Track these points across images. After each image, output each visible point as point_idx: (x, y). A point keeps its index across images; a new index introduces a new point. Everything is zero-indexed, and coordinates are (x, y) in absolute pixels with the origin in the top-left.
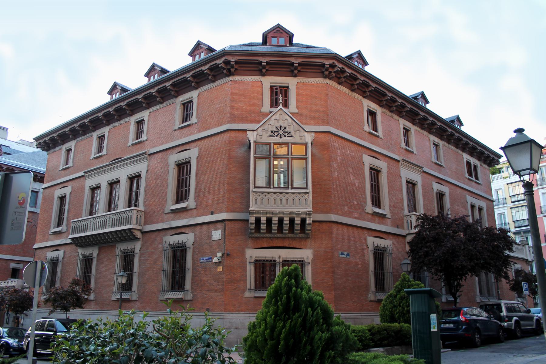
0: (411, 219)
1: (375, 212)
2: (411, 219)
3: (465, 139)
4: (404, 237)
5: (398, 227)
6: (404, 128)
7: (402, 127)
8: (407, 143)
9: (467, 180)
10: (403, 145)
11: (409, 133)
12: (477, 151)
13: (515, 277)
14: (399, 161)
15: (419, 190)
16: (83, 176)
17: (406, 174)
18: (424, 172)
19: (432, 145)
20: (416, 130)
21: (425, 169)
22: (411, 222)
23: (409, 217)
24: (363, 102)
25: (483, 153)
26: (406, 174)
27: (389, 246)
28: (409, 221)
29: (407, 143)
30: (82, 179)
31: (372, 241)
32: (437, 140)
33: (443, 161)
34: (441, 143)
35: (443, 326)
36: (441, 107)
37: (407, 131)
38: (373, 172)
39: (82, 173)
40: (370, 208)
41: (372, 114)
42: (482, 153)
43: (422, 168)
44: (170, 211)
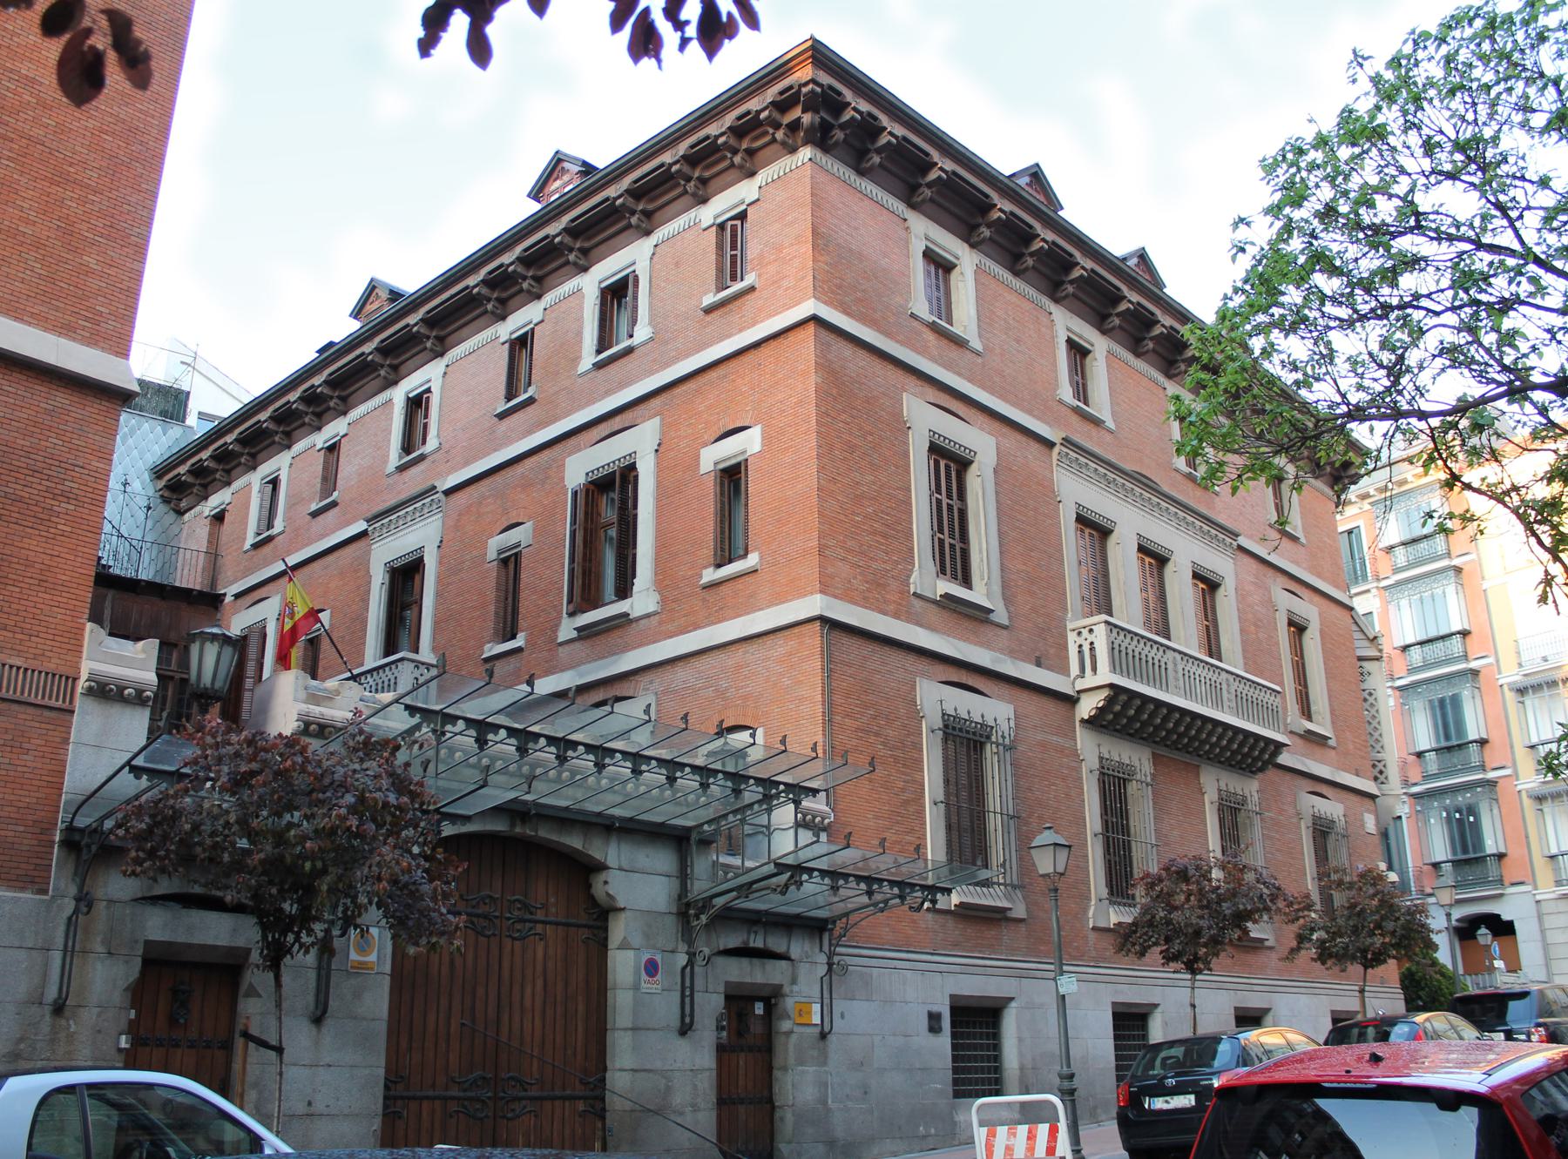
0: (1091, 638)
1: (1309, 732)
2: (1091, 638)
5: (1039, 664)
6: (1070, 342)
7: (918, 247)
8: (1081, 391)
10: (1066, 393)
11: (1089, 359)
14: (1050, 445)
15: (1226, 602)
16: (364, 534)
18: (1240, 548)
19: (918, 264)
20: (979, 270)
21: (1242, 541)
22: (1092, 649)
23: (1085, 632)
24: (1054, 316)
26: (1076, 490)
27: (1004, 727)
28: (1086, 648)
29: (1081, 391)
30: (361, 544)
34: (1100, 345)
35: (759, 1009)
37: (940, 266)
38: (1147, 560)
39: (361, 526)
41: (1078, 352)
44: (574, 634)
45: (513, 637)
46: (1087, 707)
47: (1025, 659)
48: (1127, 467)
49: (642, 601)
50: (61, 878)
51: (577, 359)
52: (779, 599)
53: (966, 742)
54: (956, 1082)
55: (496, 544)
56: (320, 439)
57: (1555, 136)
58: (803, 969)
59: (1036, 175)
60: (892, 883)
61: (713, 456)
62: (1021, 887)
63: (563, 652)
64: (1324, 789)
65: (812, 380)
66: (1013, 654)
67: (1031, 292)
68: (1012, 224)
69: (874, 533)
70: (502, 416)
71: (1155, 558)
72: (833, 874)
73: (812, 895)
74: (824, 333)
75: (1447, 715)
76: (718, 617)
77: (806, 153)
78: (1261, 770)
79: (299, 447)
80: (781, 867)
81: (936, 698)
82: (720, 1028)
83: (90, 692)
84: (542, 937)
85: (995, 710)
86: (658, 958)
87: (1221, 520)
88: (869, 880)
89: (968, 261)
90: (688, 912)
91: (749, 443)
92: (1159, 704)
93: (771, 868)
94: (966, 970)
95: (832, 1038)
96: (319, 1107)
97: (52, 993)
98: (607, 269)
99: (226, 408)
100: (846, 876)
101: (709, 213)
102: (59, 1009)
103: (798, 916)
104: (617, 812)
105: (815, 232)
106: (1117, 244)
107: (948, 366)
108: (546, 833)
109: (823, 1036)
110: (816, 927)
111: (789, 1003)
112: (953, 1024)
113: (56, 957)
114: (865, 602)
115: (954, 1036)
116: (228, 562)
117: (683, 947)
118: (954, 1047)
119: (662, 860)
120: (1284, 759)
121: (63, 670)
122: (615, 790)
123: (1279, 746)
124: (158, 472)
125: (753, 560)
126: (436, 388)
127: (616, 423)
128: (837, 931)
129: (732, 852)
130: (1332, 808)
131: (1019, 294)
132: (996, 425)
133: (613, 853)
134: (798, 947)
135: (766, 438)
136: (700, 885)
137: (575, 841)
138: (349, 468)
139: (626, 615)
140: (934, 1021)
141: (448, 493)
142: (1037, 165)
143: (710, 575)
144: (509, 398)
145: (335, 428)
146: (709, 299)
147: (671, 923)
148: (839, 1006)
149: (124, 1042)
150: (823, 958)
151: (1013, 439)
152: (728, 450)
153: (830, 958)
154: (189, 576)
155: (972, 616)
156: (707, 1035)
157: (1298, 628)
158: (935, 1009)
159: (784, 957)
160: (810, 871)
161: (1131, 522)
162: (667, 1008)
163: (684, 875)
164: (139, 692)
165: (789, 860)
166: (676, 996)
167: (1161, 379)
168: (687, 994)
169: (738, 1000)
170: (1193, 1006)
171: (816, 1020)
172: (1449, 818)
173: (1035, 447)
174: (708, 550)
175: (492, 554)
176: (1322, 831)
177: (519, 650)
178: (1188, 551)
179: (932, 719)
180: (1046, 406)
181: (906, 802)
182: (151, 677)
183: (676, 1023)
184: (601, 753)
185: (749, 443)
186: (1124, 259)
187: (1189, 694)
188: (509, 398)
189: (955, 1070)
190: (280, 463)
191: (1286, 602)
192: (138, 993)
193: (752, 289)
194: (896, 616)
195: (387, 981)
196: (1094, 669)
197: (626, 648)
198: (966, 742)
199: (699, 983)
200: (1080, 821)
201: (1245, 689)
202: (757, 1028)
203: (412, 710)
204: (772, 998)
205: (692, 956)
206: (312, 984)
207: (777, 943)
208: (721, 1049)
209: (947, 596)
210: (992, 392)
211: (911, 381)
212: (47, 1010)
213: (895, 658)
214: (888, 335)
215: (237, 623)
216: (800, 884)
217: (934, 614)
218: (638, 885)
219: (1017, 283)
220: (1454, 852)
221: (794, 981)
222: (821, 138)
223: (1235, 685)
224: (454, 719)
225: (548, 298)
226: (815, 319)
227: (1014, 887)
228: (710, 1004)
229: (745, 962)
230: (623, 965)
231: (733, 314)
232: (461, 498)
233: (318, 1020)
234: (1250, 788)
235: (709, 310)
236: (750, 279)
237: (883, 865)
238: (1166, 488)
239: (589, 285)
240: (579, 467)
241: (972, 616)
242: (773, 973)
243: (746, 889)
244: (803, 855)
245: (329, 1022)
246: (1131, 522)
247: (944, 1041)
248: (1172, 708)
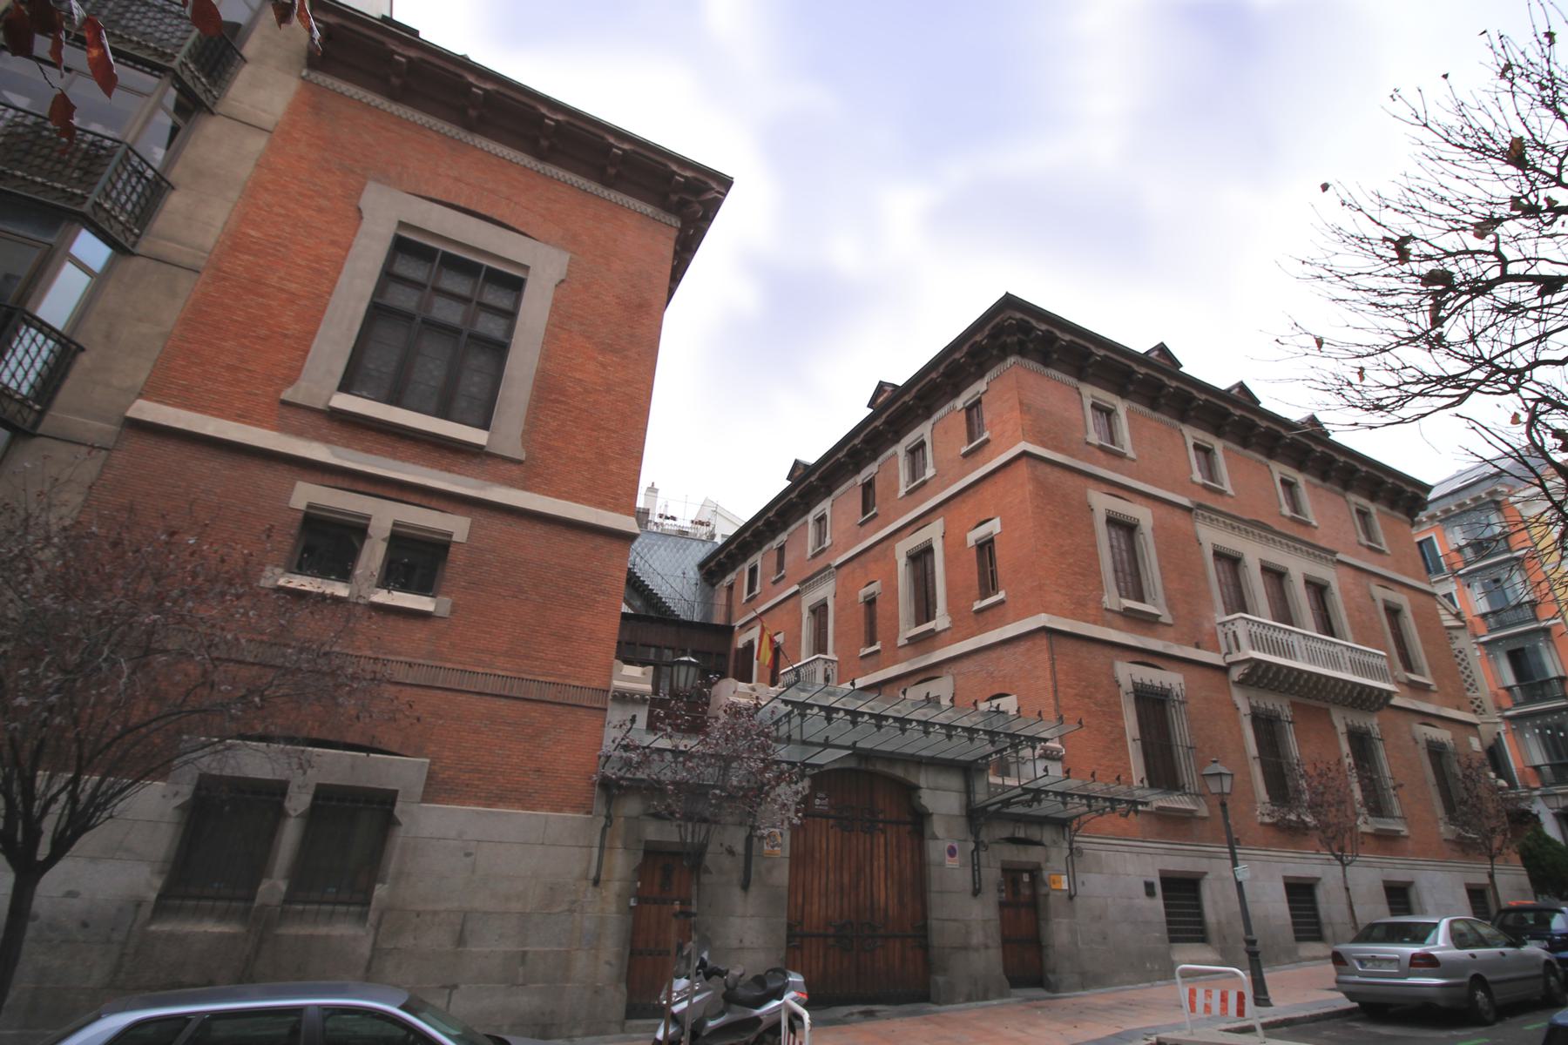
3: (1410, 489)
4: (1225, 670)
7: (1088, 403)
8: (1295, 505)
9: (1365, 551)
12: (1165, 392)
13: (643, 664)
16: (797, 593)
17: (1212, 536)
20: (1129, 411)
21: (1339, 556)
25: (1401, 491)
26: (1212, 536)
27: (1177, 689)
31: (1128, 673)
32: (1364, 502)
33: (1383, 540)
35: (1026, 878)
36: (1209, 364)
37: (1107, 413)
39: (796, 587)
40: (1113, 599)
41: (1288, 485)
42: (1399, 492)
43: (1334, 553)
45: (872, 643)
46: (1236, 673)
47: (1188, 644)
48: (1246, 517)
49: (941, 621)
50: (599, 807)
51: (897, 490)
52: (1019, 617)
53: (1152, 703)
54: (1170, 931)
55: (863, 592)
56: (775, 544)
57: (1051, 977)
58: (1054, 852)
59: (1162, 349)
60: (1105, 799)
61: (973, 537)
62: (1202, 795)
63: (901, 652)
64: (1434, 722)
65: (1030, 487)
66: (1179, 641)
67: (1166, 418)
68: (1153, 381)
69: (1075, 573)
70: (861, 524)
71: (1275, 575)
72: (1063, 795)
73: (1049, 807)
74: (1032, 462)
75: (1520, 659)
76: (982, 630)
77: (1011, 360)
78: (1378, 709)
79: (766, 548)
80: (1026, 791)
81: (1128, 673)
82: (1000, 891)
83: (615, 698)
84: (884, 832)
85: (1170, 679)
86: (956, 845)
87: (1322, 544)
88: (1088, 797)
89: (1122, 407)
90: (975, 816)
91: (995, 526)
92: (1291, 669)
93: (1019, 791)
94: (1169, 852)
95: (1077, 899)
96: (747, 943)
97: (593, 873)
98: (910, 439)
99: (731, 531)
100: (1072, 795)
101: (960, 403)
102: (596, 882)
103: (1046, 817)
104: (924, 753)
105: (1021, 403)
106: (1223, 382)
107: (1114, 470)
108: (880, 767)
109: (1071, 898)
110: (1062, 824)
111: (1046, 874)
112: (1164, 889)
113: (596, 851)
114: (1073, 615)
115: (1165, 898)
116: (736, 608)
117: (971, 838)
118: (1166, 906)
119: (956, 782)
120: (1395, 701)
121: (603, 687)
122: (914, 743)
123: (1390, 694)
124: (701, 566)
125: (1001, 595)
126: (828, 513)
127: (920, 523)
128: (1074, 826)
129: (1004, 771)
130: (1442, 735)
131: (1158, 423)
132: (1150, 502)
133: (924, 779)
134: (1048, 835)
135: (1002, 524)
136: (980, 796)
137: (899, 772)
138: (789, 558)
139: (932, 630)
140: (1149, 889)
141: (838, 567)
142: (726, 182)
143: (978, 605)
144: (864, 513)
145: (782, 537)
146: (964, 450)
147: (962, 822)
148: (1080, 877)
149: (633, 903)
150: (1066, 845)
151: (1163, 510)
152: (982, 531)
153: (1071, 843)
154: (719, 619)
155: (1146, 622)
156: (991, 897)
157: (1393, 612)
158: (1150, 879)
159: (1039, 843)
160: (1047, 792)
161: (1254, 553)
162: (963, 878)
163: (969, 791)
164: (643, 696)
165: (1031, 786)
166: (969, 870)
167: (1264, 459)
168: (976, 868)
169: (1011, 873)
170: (1347, 889)
171: (1065, 886)
172: (1542, 734)
173: (1179, 513)
174: (976, 591)
175: (861, 599)
176: (1436, 751)
177: (1002, 602)
178: (1299, 567)
179: (1127, 685)
180: (1185, 486)
181: (1114, 741)
182: (648, 687)
183: (969, 886)
184: (903, 722)
185: (995, 526)
186: (1229, 390)
187: (1312, 660)
188: (864, 513)
189: (1169, 923)
190: (757, 559)
191: (1380, 593)
192: (641, 871)
193: (987, 441)
194: (1095, 623)
195: (787, 862)
196: (1238, 648)
197: (934, 649)
198: (1152, 703)
199: (983, 861)
200: (1242, 749)
201: (1357, 656)
202: (1026, 892)
203: (786, 702)
204: (1035, 872)
205: (977, 844)
206: (742, 865)
207: (1034, 833)
208: (1002, 905)
209: (1128, 609)
210: (1146, 482)
211: (1090, 482)
212: (590, 883)
213: (1097, 651)
214: (1073, 456)
215: (741, 641)
216: (1040, 801)
217: (1119, 621)
218: (942, 800)
219: (1156, 415)
220: (1550, 757)
221: (1047, 860)
222: (1022, 351)
223: (1347, 654)
224: (811, 706)
225: (880, 459)
226: (1025, 454)
227: (1198, 795)
228: (991, 874)
229: (1013, 847)
230: (936, 850)
231: (979, 457)
232: (845, 570)
233: (745, 886)
234: (1373, 723)
235: (965, 455)
236: (986, 435)
237: (1097, 788)
238: (1277, 528)
239: (900, 449)
240: (903, 548)
241: (1146, 622)
242: (1032, 855)
243: (1007, 803)
244: (1041, 782)
245: (753, 889)
246: (1254, 553)
247: (1158, 902)
248: (1301, 672)
